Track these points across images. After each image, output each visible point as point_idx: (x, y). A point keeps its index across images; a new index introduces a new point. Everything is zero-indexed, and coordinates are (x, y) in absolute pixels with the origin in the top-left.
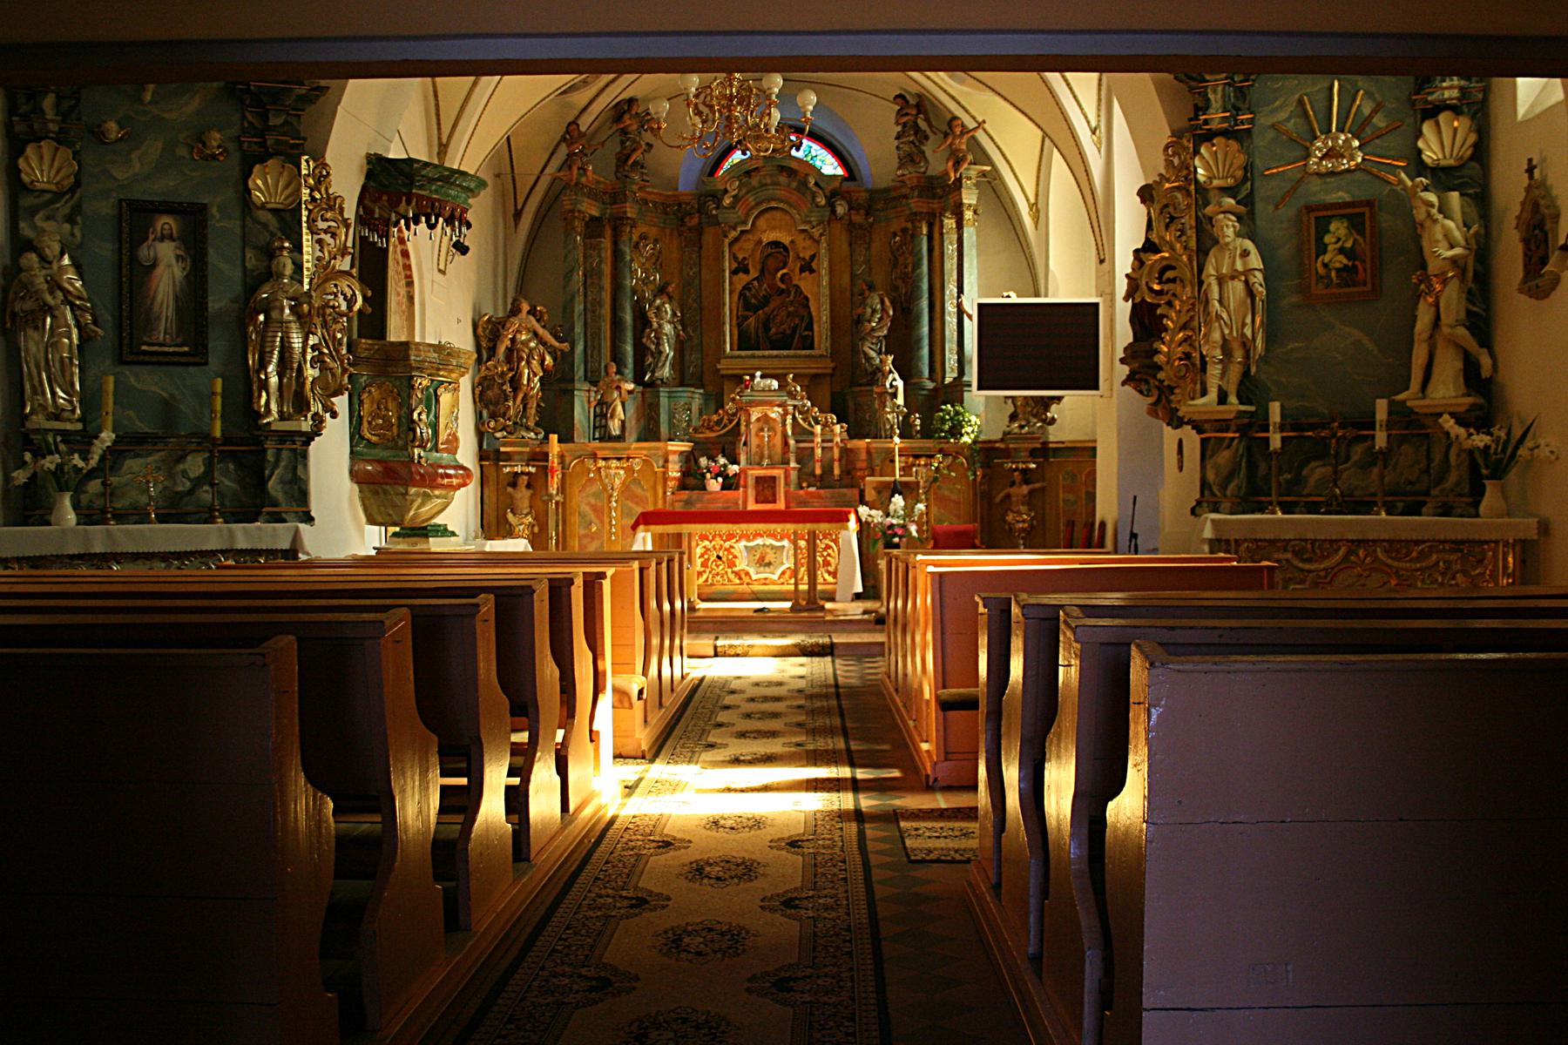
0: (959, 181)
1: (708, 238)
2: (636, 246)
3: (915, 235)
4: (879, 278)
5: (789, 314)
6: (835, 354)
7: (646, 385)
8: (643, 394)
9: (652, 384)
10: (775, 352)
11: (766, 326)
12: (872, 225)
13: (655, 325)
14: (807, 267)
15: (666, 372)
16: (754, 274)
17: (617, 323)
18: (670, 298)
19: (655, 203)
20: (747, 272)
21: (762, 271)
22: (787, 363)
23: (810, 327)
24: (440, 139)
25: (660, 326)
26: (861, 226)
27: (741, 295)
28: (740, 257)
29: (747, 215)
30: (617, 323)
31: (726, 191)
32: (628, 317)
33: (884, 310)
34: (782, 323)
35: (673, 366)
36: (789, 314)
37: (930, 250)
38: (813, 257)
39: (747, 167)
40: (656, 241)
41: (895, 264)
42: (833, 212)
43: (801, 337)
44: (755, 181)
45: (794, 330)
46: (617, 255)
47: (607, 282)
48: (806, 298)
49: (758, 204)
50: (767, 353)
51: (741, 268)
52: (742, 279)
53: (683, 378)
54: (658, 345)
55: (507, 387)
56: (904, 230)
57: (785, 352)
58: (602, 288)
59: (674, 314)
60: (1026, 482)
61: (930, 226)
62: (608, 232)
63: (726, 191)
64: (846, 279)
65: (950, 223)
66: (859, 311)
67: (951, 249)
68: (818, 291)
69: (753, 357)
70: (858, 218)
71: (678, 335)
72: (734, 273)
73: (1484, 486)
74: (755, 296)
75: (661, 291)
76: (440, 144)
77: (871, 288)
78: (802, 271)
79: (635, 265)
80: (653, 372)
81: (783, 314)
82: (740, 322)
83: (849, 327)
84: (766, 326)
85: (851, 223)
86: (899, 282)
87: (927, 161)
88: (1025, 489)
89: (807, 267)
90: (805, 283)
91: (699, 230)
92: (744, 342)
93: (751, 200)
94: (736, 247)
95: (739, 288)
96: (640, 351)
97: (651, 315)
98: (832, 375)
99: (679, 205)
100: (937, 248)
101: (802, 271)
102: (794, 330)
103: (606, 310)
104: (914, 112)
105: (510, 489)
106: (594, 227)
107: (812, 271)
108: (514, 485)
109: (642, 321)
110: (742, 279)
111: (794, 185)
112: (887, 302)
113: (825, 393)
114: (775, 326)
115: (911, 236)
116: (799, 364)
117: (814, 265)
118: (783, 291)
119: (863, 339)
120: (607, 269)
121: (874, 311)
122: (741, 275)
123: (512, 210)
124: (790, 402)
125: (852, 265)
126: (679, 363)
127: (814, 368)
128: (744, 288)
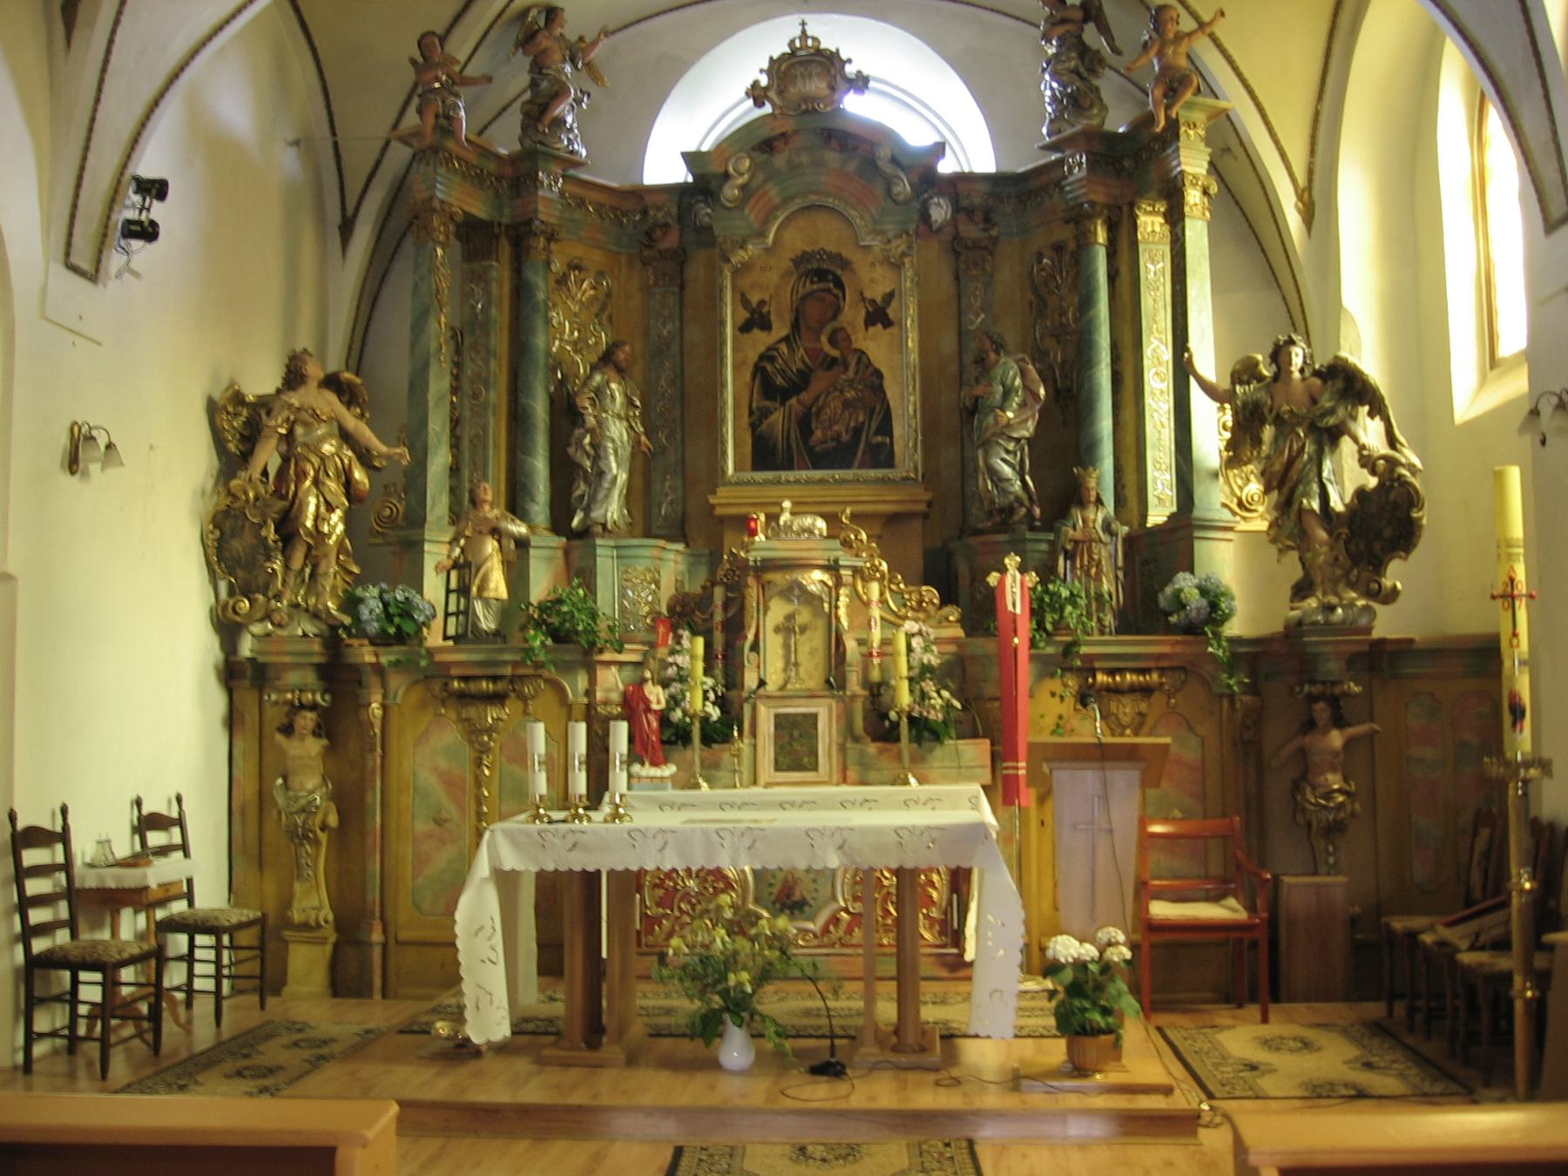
0: (1173, 126)
1: (696, 271)
2: (562, 281)
3: (1084, 243)
4: (1010, 332)
5: (847, 404)
6: (930, 477)
7: (573, 535)
8: (567, 552)
9: (585, 533)
10: (818, 474)
11: (804, 424)
12: (995, 240)
13: (591, 421)
14: (878, 316)
15: (612, 509)
16: (780, 330)
17: (518, 419)
18: (621, 371)
19: (599, 207)
20: (766, 326)
21: (795, 326)
22: (843, 493)
23: (886, 427)
24: (343, 209)
25: (600, 423)
26: (976, 246)
27: (758, 370)
28: (754, 299)
29: (766, 222)
30: (518, 419)
31: (726, 176)
32: (540, 409)
33: (1030, 392)
34: (832, 422)
35: (628, 499)
36: (847, 404)
37: (1112, 278)
38: (889, 297)
39: (766, 132)
40: (601, 274)
41: (1039, 306)
42: (925, 217)
43: (868, 444)
44: (780, 160)
45: (857, 432)
46: (521, 292)
47: (500, 341)
48: (879, 374)
49: (786, 201)
50: (804, 474)
51: (756, 320)
52: (761, 340)
53: (649, 521)
54: (596, 459)
55: (270, 533)
56: (1058, 248)
57: (838, 474)
58: (490, 353)
59: (630, 403)
60: (1339, 722)
61: (1112, 228)
62: (505, 249)
63: (726, 176)
64: (948, 342)
65: (1151, 223)
66: (979, 390)
67: (1154, 270)
68: (898, 357)
69: (778, 482)
70: (971, 231)
71: (636, 444)
72: (745, 328)
73: (671, 609)
74: (782, 373)
75: (607, 359)
76: (344, 216)
77: (999, 347)
78: (870, 320)
79: (556, 316)
80: (587, 510)
81: (835, 405)
82: (757, 419)
83: (961, 420)
84: (804, 424)
85: (956, 237)
86: (1050, 343)
87: (1104, 108)
88: (1336, 739)
89: (878, 316)
90: (875, 345)
91: (680, 257)
92: (765, 455)
93: (773, 193)
94: (746, 282)
95: (753, 356)
96: (564, 471)
97: (584, 403)
98: (925, 516)
99: (645, 212)
100: (1124, 270)
101: (870, 320)
102: (857, 432)
103: (497, 397)
104: (1078, 15)
105: (279, 738)
106: (475, 237)
107: (887, 323)
108: (288, 730)
109: (566, 414)
110: (761, 340)
111: (852, 166)
112: (1034, 375)
113: (915, 553)
114: (817, 420)
115: (1076, 257)
116: (864, 493)
117: (891, 312)
118: (834, 361)
119: (987, 445)
120: (501, 317)
121: (1008, 393)
122: (756, 332)
123: (335, 218)
124: (846, 560)
125: (960, 313)
126: (640, 495)
127: (889, 502)
128: (762, 357)
